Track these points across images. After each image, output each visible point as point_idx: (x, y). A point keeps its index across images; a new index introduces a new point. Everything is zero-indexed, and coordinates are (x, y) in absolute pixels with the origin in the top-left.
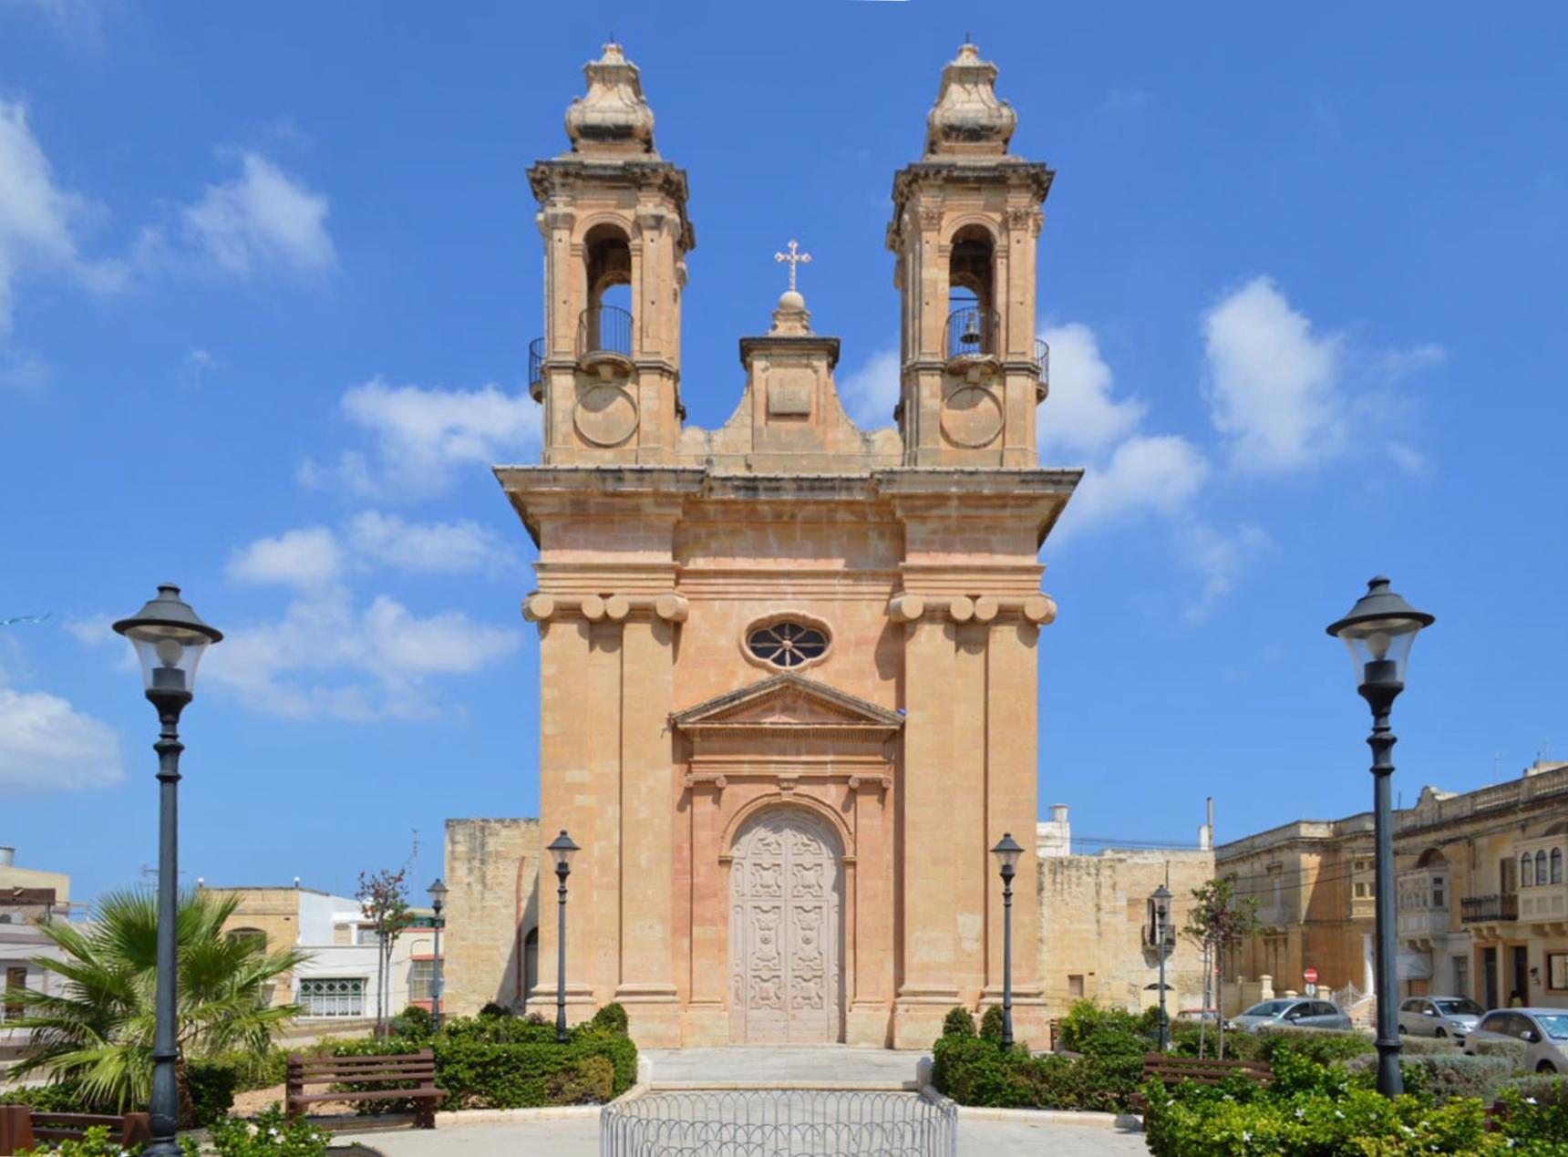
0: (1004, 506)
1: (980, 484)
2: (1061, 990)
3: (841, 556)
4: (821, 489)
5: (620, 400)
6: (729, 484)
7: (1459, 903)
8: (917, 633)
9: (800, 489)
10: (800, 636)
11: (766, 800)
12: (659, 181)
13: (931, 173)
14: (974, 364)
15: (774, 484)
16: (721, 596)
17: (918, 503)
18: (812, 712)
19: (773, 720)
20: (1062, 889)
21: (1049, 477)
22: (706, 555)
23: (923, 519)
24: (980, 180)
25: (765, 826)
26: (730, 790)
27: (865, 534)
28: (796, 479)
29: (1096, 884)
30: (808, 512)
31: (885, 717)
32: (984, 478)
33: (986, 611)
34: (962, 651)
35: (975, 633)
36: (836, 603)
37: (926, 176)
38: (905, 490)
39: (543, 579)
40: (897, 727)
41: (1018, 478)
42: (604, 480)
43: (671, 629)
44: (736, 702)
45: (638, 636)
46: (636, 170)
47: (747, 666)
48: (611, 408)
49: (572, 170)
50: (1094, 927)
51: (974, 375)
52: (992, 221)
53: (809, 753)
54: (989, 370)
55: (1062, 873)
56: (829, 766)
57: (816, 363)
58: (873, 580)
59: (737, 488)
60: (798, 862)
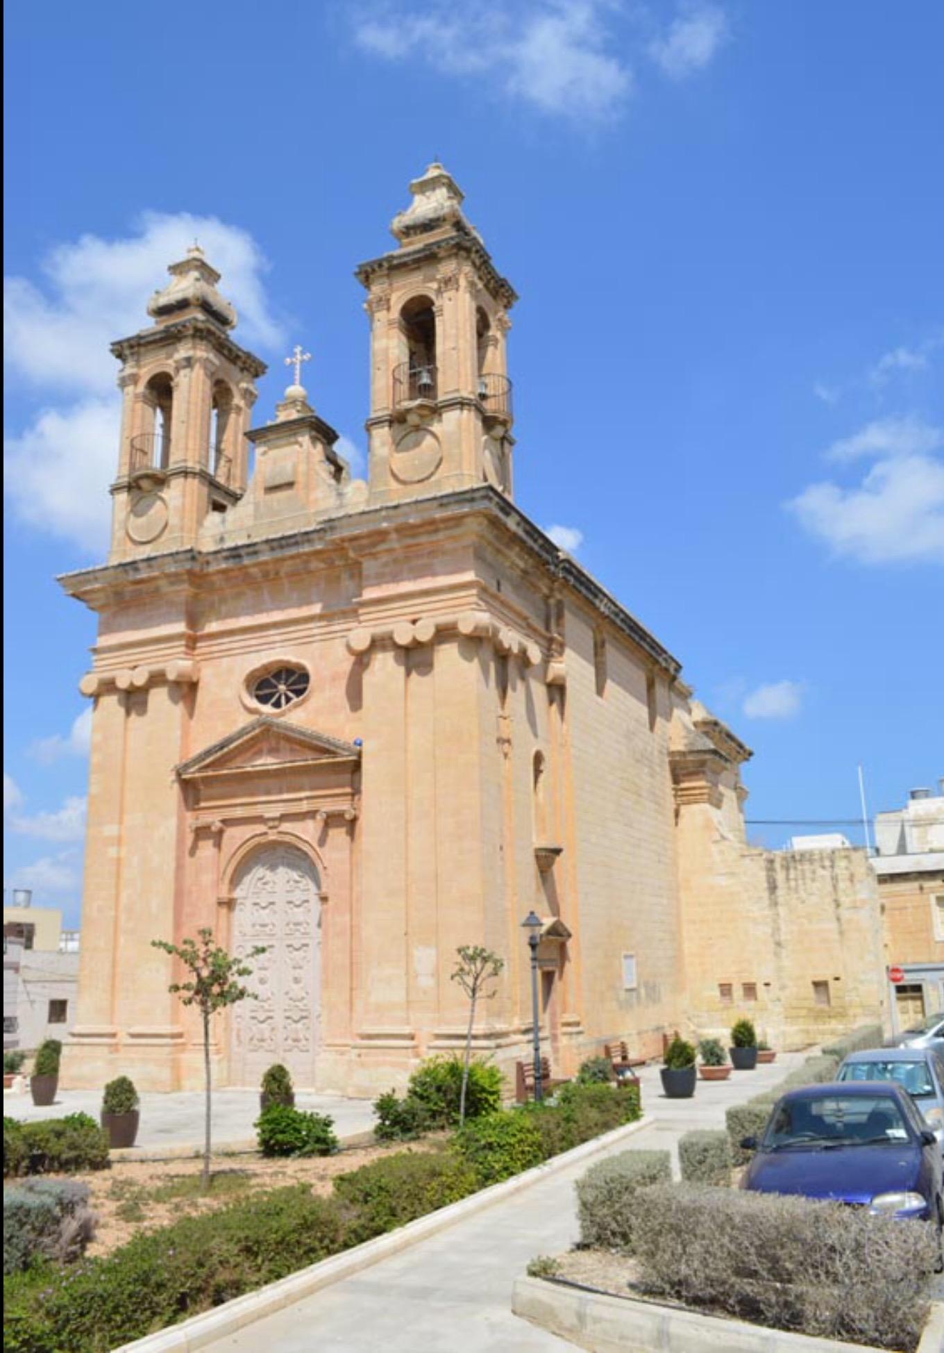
0: (436, 531)
1: (406, 515)
2: (805, 999)
3: (320, 601)
4: (288, 545)
5: (159, 503)
6: (219, 556)
7: (54, 1026)
8: (372, 664)
9: (273, 549)
10: (292, 679)
11: (257, 840)
12: (191, 332)
13: (376, 267)
14: (408, 411)
15: (251, 549)
16: (228, 653)
17: (364, 542)
18: (292, 750)
19: (267, 762)
20: (797, 886)
21: (462, 497)
22: (218, 619)
23: (374, 556)
24: (417, 261)
25: (263, 865)
26: (230, 832)
27: (338, 578)
28: (267, 541)
29: (832, 878)
30: (286, 567)
31: (344, 749)
32: (406, 509)
33: (425, 633)
34: (414, 675)
35: (416, 657)
36: (315, 645)
37: (374, 271)
38: (346, 533)
39: (96, 660)
40: (354, 758)
41: (435, 503)
42: (126, 571)
43: (186, 690)
44: (226, 750)
45: (159, 698)
46: (173, 329)
47: (245, 713)
48: (152, 512)
49: (133, 342)
50: (834, 925)
51: (413, 419)
52: (430, 289)
53: (289, 791)
54: (425, 412)
55: (795, 868)
56: (305, 802)
57: (300, 439)
58: (345, 618)
59: (226, 558)
60: (289, 899)
